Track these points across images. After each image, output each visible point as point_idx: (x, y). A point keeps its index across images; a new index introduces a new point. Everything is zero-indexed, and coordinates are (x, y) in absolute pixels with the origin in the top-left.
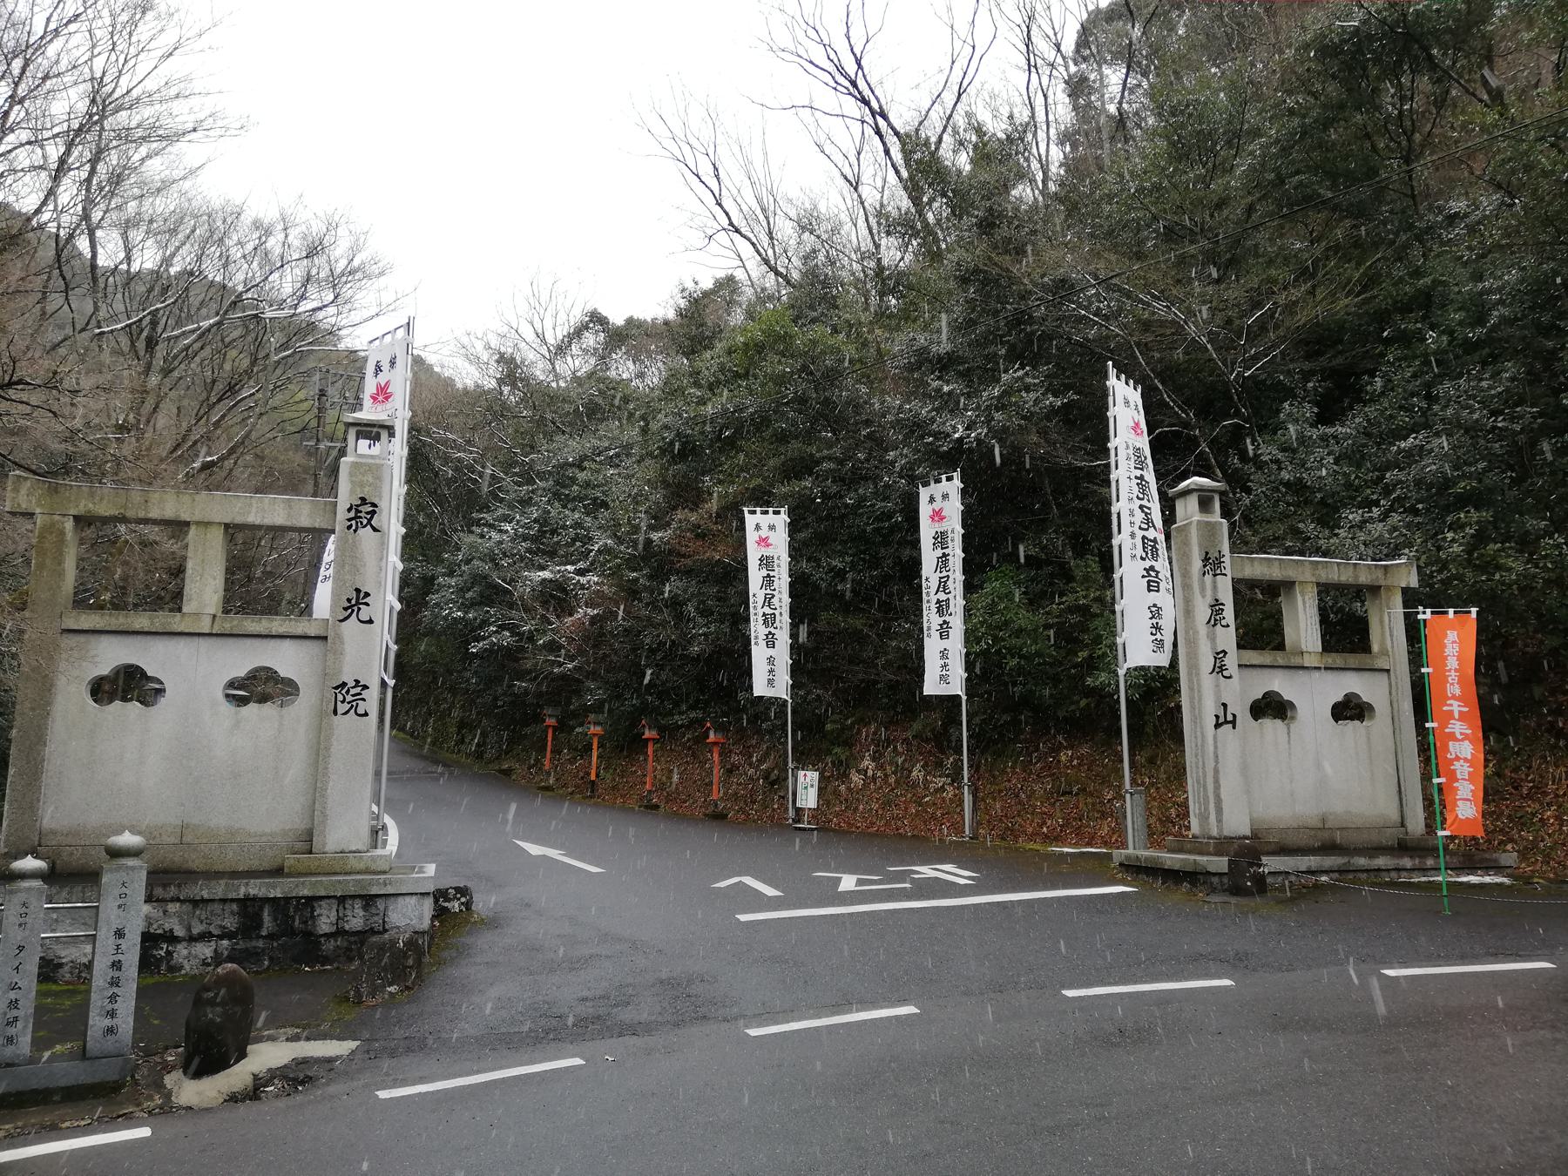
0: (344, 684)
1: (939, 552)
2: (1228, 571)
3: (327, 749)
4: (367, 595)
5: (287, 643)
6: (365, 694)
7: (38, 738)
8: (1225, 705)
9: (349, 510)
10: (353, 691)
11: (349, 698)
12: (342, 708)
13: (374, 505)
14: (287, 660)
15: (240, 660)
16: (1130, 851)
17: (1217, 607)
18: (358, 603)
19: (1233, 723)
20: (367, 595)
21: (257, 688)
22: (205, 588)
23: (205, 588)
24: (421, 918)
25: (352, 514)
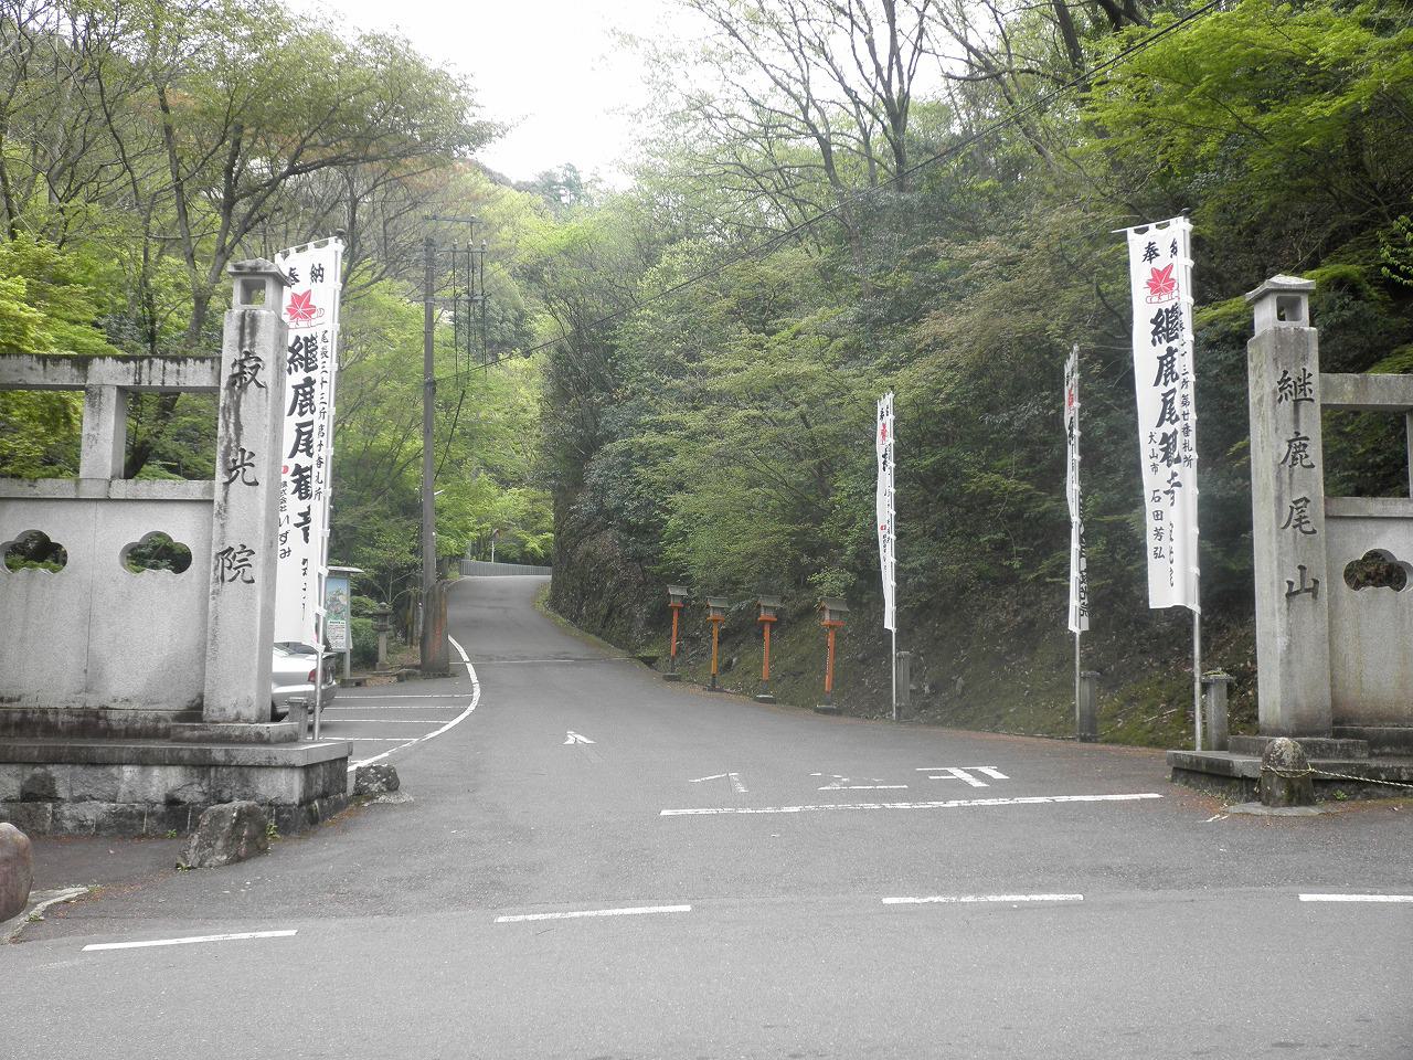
0: (231, 549)
1: (1162, 349)
2: (1316, 395)
3: (1368, 796)
4: (252, 454)
5: (178, 508)
6: (251, 560)
7: (310, 843)
8: (1302, 568)
9: (234, 365)
10: (239, 557)
11: (236, 564)
12: (229, 575)
13: (258, 359)
14: (182, 528)
15: (136, 527)
16: (1198, 752)
17: (1298, 443)
18: (243, 464)
19: (1314, 591)
20: (252, 454)
21: (161, 555)
22: (102, 438)
23: (102, 438)
24: (291, 791)
25: (237, 370)
